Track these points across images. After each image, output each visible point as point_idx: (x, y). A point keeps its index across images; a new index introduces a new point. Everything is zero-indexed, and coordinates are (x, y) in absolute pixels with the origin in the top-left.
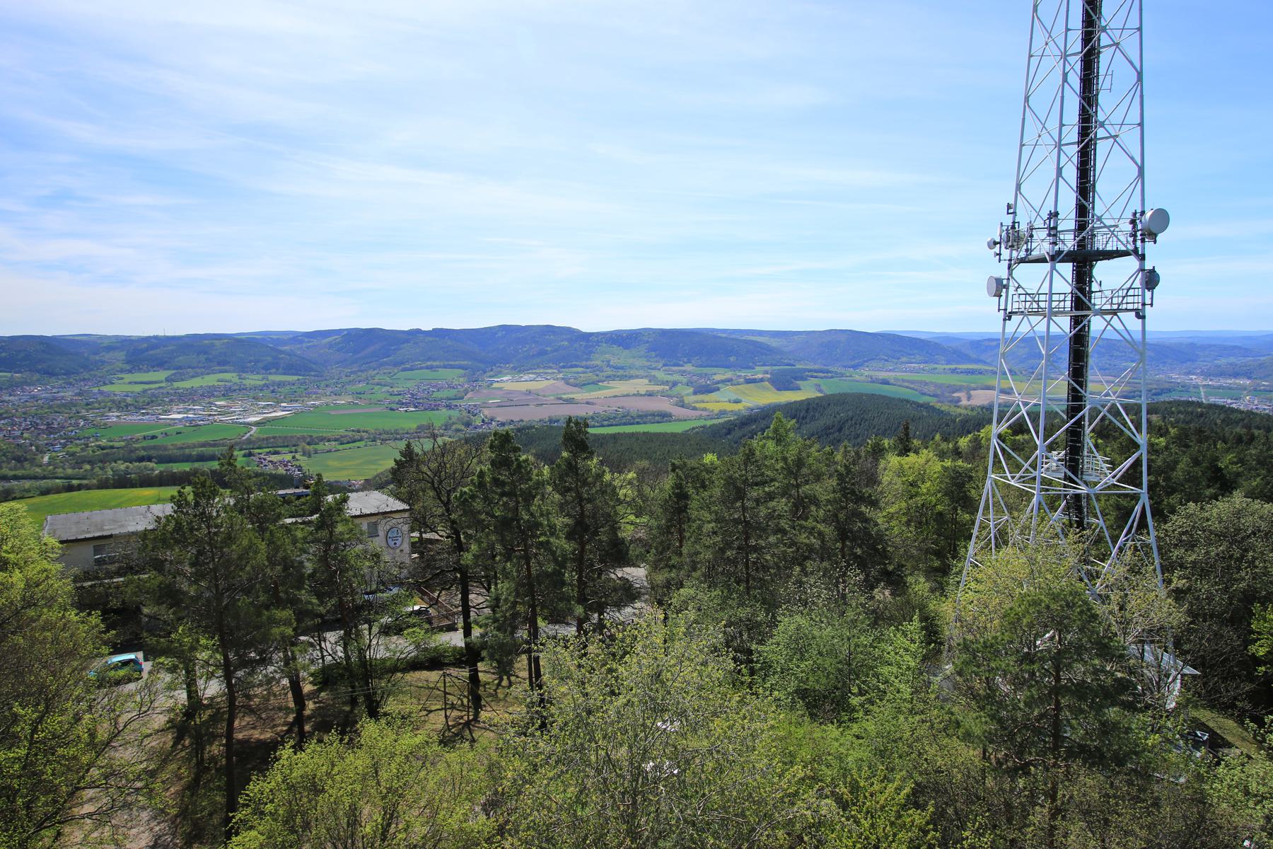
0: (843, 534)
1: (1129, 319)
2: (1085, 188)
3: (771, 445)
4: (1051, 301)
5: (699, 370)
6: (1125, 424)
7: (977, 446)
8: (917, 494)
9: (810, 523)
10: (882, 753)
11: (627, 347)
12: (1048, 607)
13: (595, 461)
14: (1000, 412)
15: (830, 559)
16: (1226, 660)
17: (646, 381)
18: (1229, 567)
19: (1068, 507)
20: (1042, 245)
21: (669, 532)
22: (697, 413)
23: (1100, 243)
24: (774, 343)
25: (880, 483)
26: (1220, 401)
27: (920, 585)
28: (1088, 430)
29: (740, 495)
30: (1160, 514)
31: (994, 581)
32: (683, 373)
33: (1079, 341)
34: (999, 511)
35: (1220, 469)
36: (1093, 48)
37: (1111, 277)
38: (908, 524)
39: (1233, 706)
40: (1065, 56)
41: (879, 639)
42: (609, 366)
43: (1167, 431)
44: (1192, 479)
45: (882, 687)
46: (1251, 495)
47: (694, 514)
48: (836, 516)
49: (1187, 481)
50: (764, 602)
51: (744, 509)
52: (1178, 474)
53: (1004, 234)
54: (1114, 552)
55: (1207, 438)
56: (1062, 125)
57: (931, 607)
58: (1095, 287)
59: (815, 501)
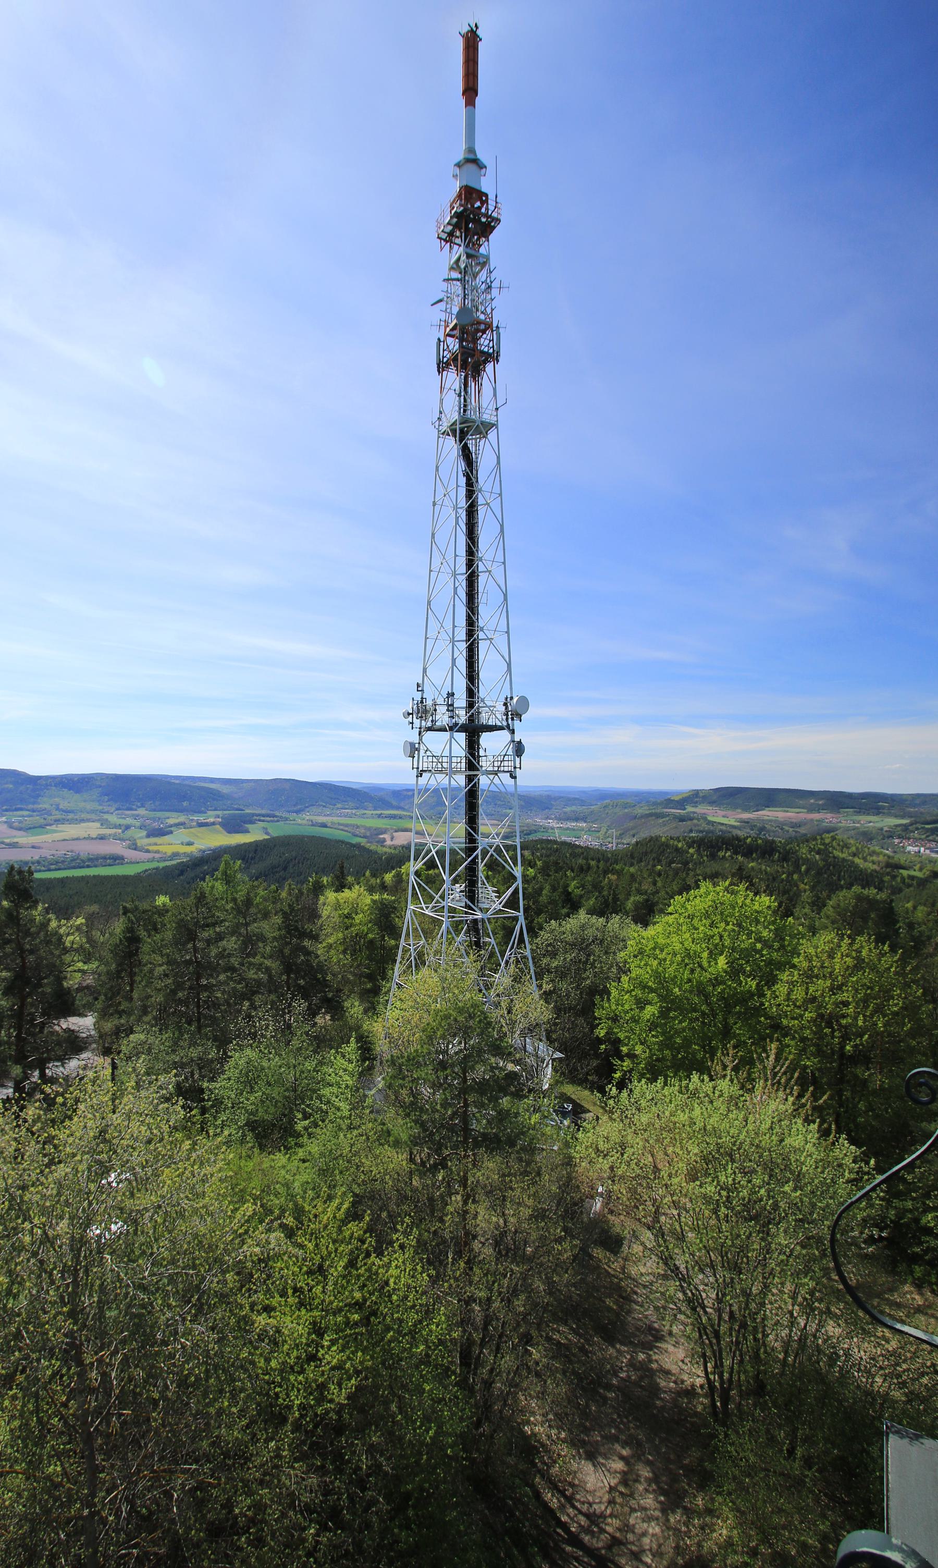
0: (288, 968)
1: (505, 778)
2: (472, 675)
3: (220, 887)
4: (451, 762)
5: (152, 814)
6: (506, 861)
7: (400, 881)
8: (351, 925)
9: (258, 959)
10: (324, 1172)
11: (78, 791)
12: (455, 1020)
13: (40, 908)
14: (416, 850)
15: (276, 991)
16: (581, 1043)
17: (98, 825)
18: (579, 969)
19: (468, 931)
20: (443, 718)
21: (119, 977)
22: (150, 856)
23: (485, 718)
24: (225, 790)
25: (320, 916)
26: (568, 840)
27: (354, 1008)
28: (481, 866)
29: (192, 937)
30: (533, 931)
31: (412, 1002)
32: (136, 817)
33: (472, 795)
34: (417, 937)
35: (570, 894)
36: (473, 572)
37: (493, 744)
38: (344, 952)
39: (586, 1080)
40: (455, 575)
41: (321, 1063)
42: (58, 809)
43: (535, 864)
44: (552, 902)
45: (324, 1107)
46: (591, 912)
47: (145, 958)
48: (281, 951)
49: (549, 903)
50: (215, 1039)
51: (196, 950)
52: (543, 899)
53: (415, 707)
54: (503, 964)
55: (561, 868)
56: (454, 626)
57: (365, 1027)
58: (482, 753)
59: (262, 938)
